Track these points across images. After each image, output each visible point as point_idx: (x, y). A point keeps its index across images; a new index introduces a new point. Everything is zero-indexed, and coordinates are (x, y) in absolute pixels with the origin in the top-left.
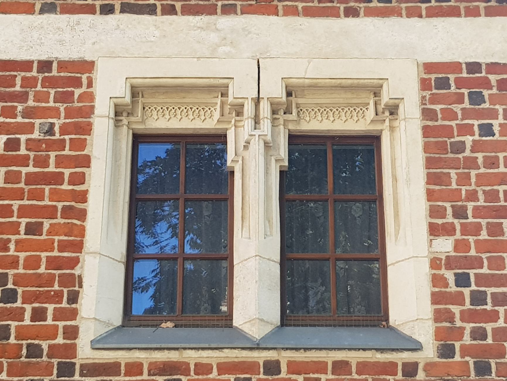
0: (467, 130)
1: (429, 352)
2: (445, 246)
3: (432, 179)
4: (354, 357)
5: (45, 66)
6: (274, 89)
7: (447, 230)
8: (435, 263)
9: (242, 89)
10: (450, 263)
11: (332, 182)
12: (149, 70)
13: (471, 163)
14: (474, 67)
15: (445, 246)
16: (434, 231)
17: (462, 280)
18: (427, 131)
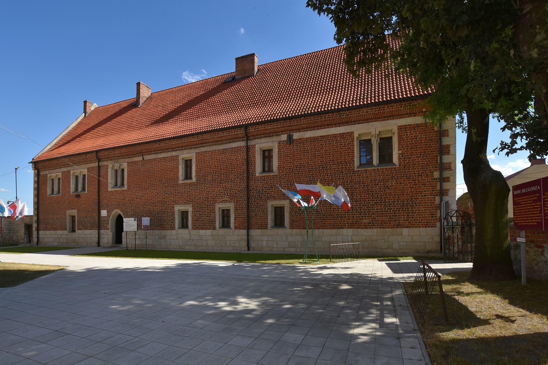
0: (404, 135)
1: (398, 166)
2: (400, 152)
3: (399, 143)
4: (388, 167)
5: (348, 133)
6: (377, 132)
7: (401, 150)
8: (399, 154)
9: (373, 133)
10: (401, 154)
11: (155, 155)
12: (360, 132)
13: (405, 140)
14: (405, 125)
15: (400, 152)
16: (399, 150)
17: (402, 156)
18: (398, 136)
